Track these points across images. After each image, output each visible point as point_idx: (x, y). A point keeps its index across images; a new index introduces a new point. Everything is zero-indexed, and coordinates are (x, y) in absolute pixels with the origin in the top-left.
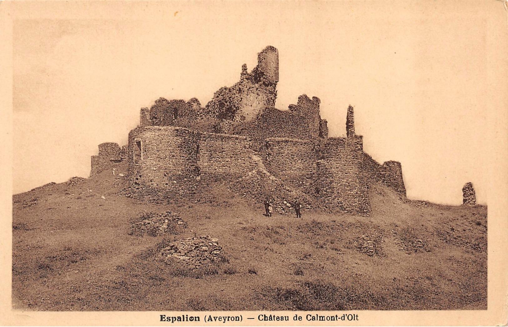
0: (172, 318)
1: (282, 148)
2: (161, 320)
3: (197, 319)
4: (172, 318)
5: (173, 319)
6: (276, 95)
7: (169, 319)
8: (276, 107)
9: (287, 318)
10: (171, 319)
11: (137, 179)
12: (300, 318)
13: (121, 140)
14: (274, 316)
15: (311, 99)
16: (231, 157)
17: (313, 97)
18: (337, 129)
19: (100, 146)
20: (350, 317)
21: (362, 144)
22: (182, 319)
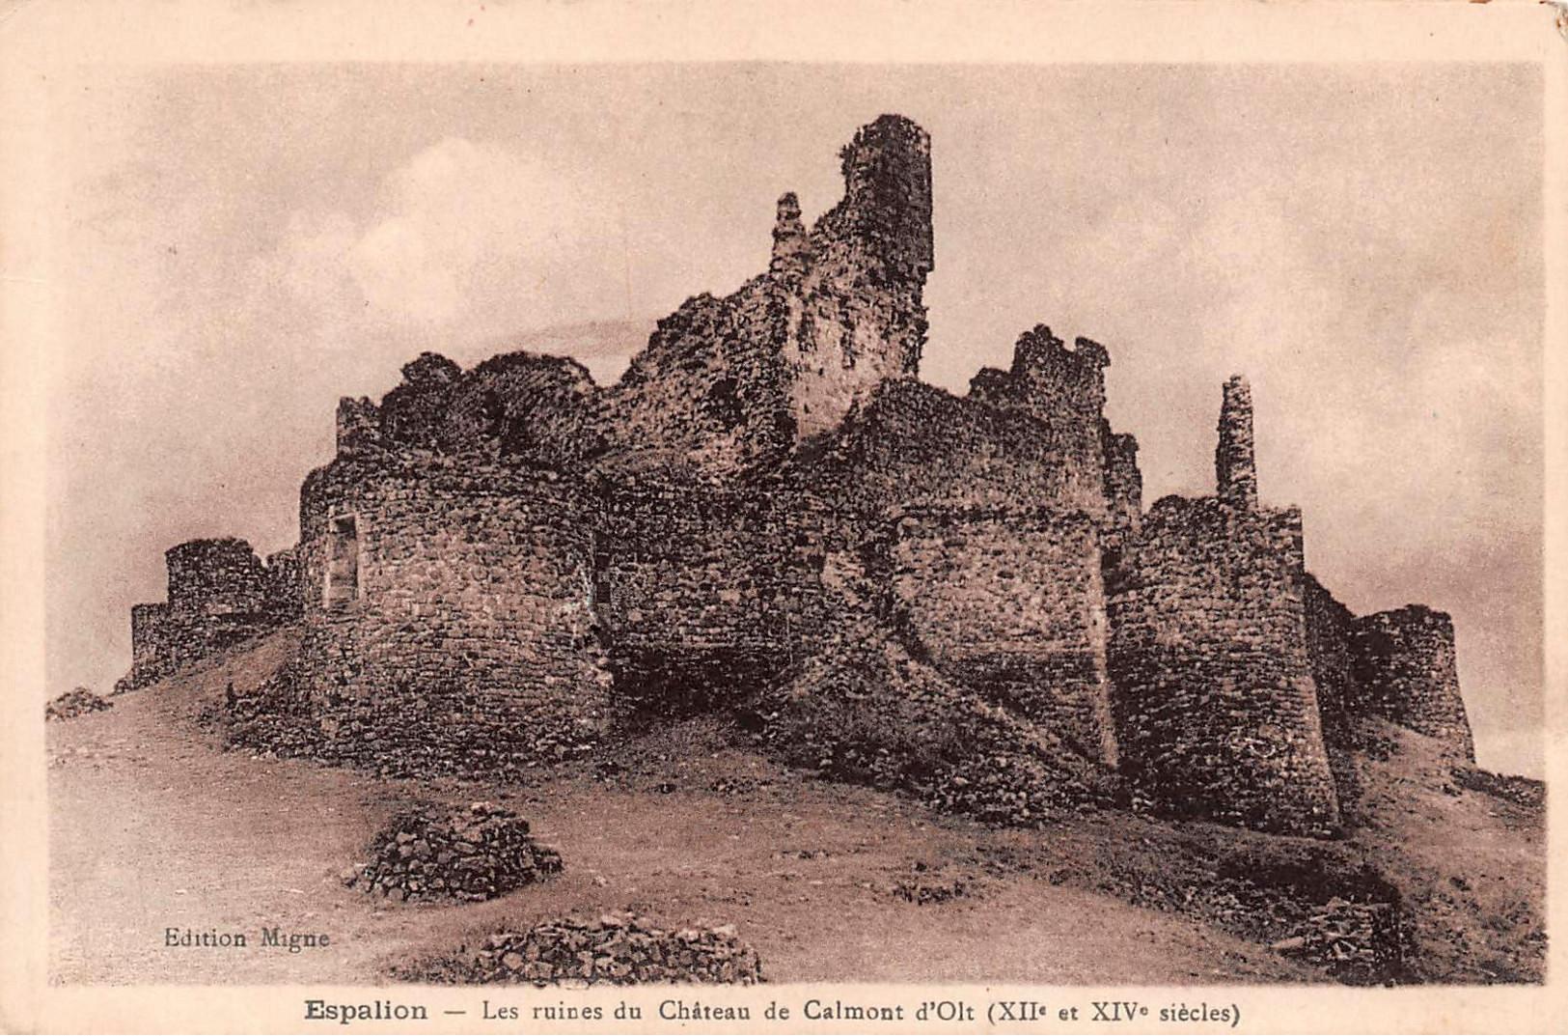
0: (345, 1009)
1: (961, 546)
2: (309, 1016)
3: (419, 1013)
4: (345, 1009)
5: (346, 1014)
6: (923, 326)
7: (331, 1012)
8: (923, 377)
9: (745, 1014)
10: (340, 1011)
11: (343, 682)
12: (784, 1014)
13: (1006, 364)
14: (707, 1009)
15: (1070, 346)
16: (745, 585)
17: (1080, 341)
18: (1174, 466)
19: (172, 555)
20: (947, 1011)
21: (1299, 527)
22: (374, 1014)
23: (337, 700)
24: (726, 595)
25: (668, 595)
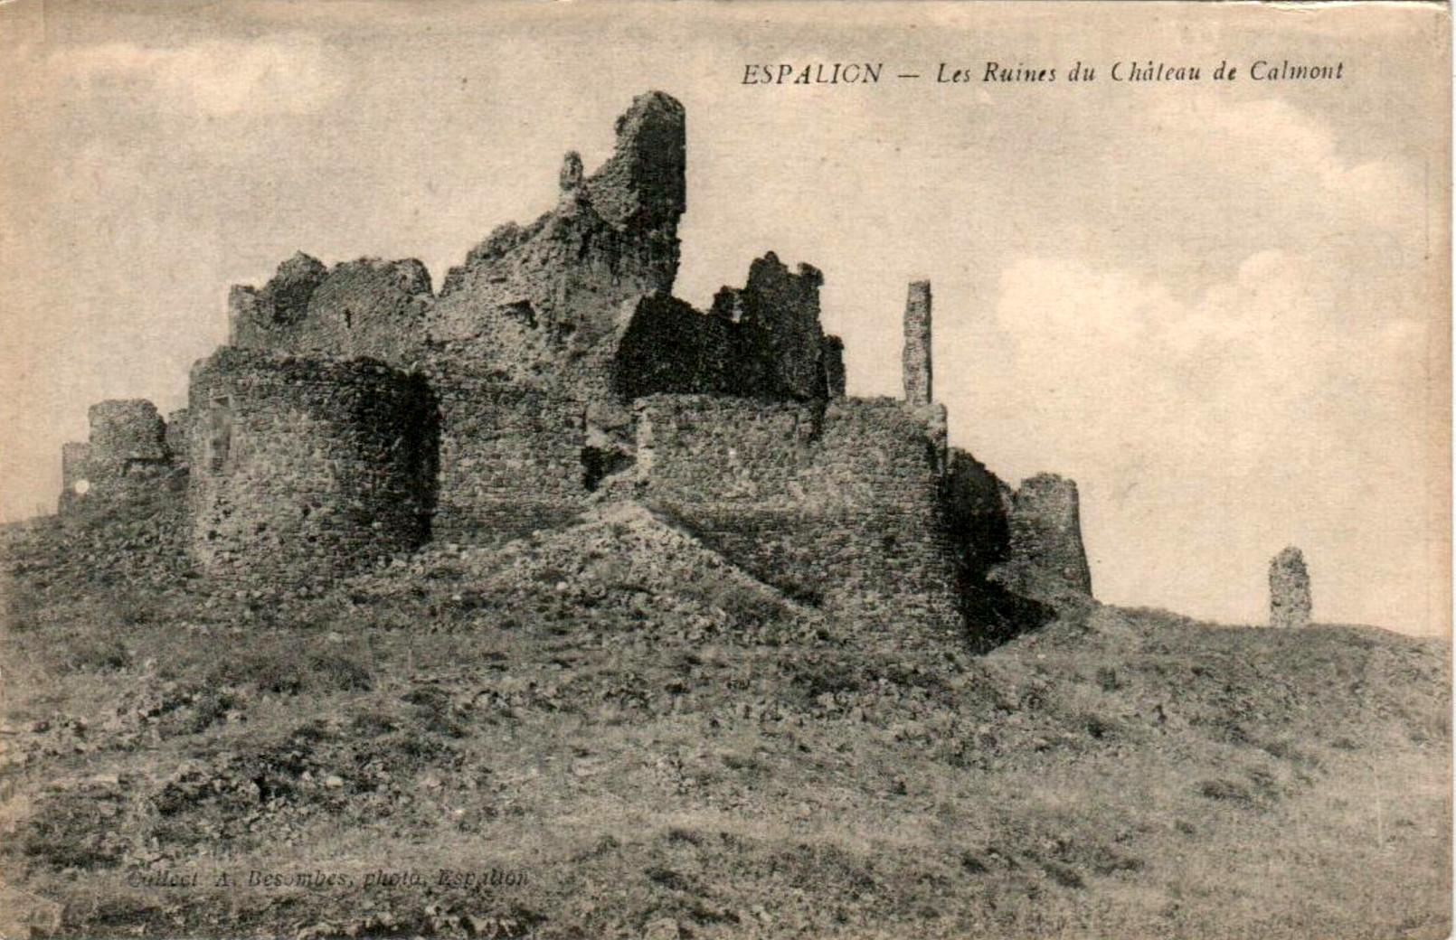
15: (794, 270)
23: (213, 535)
24: (510, 463)
25: (467, 462)
